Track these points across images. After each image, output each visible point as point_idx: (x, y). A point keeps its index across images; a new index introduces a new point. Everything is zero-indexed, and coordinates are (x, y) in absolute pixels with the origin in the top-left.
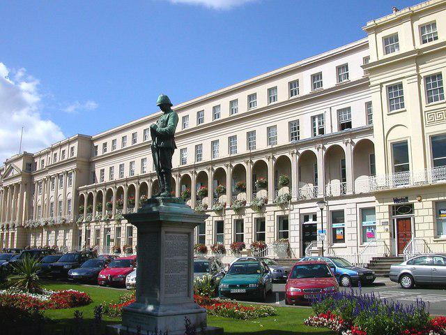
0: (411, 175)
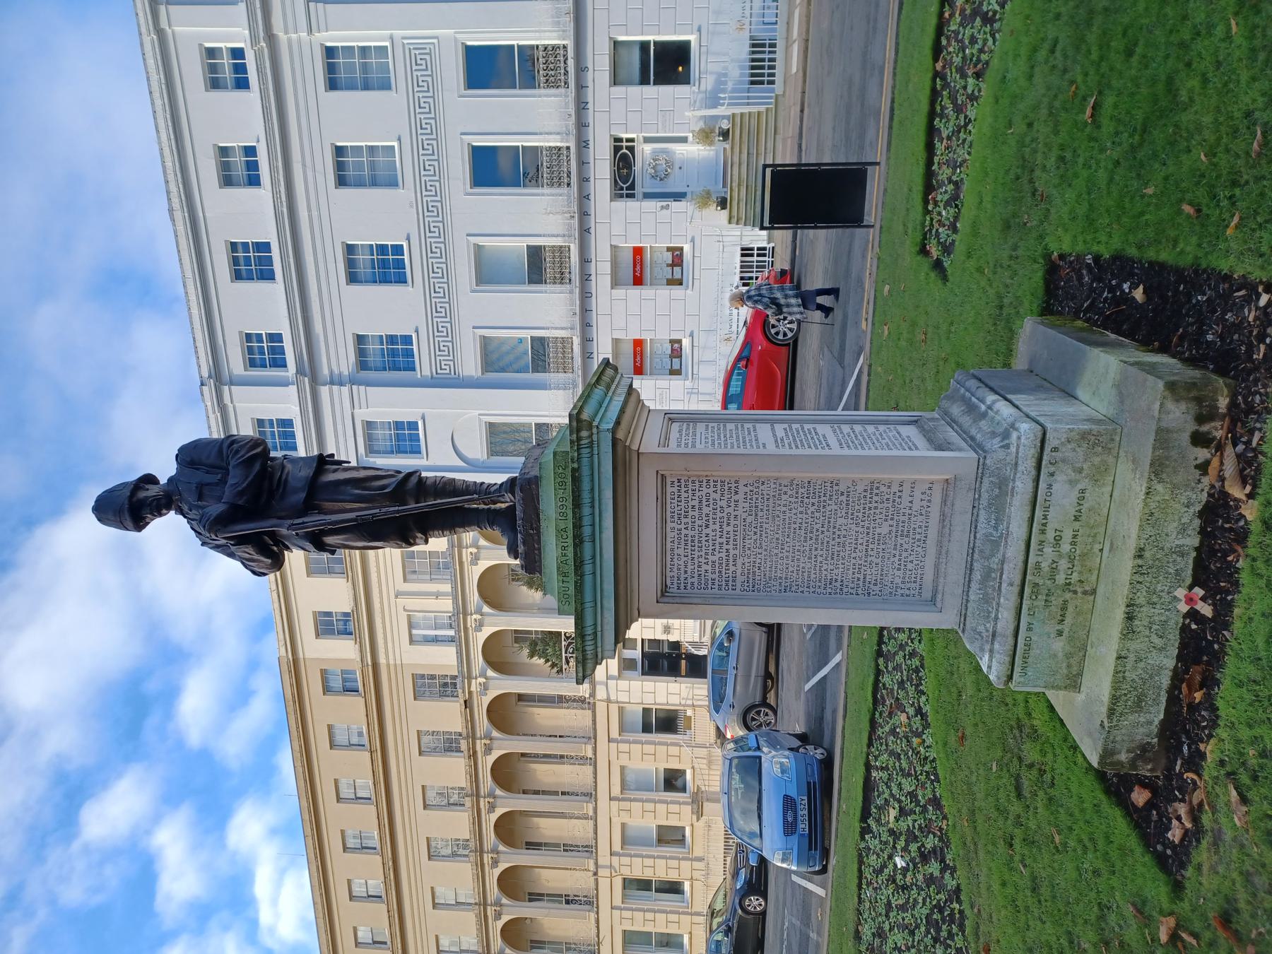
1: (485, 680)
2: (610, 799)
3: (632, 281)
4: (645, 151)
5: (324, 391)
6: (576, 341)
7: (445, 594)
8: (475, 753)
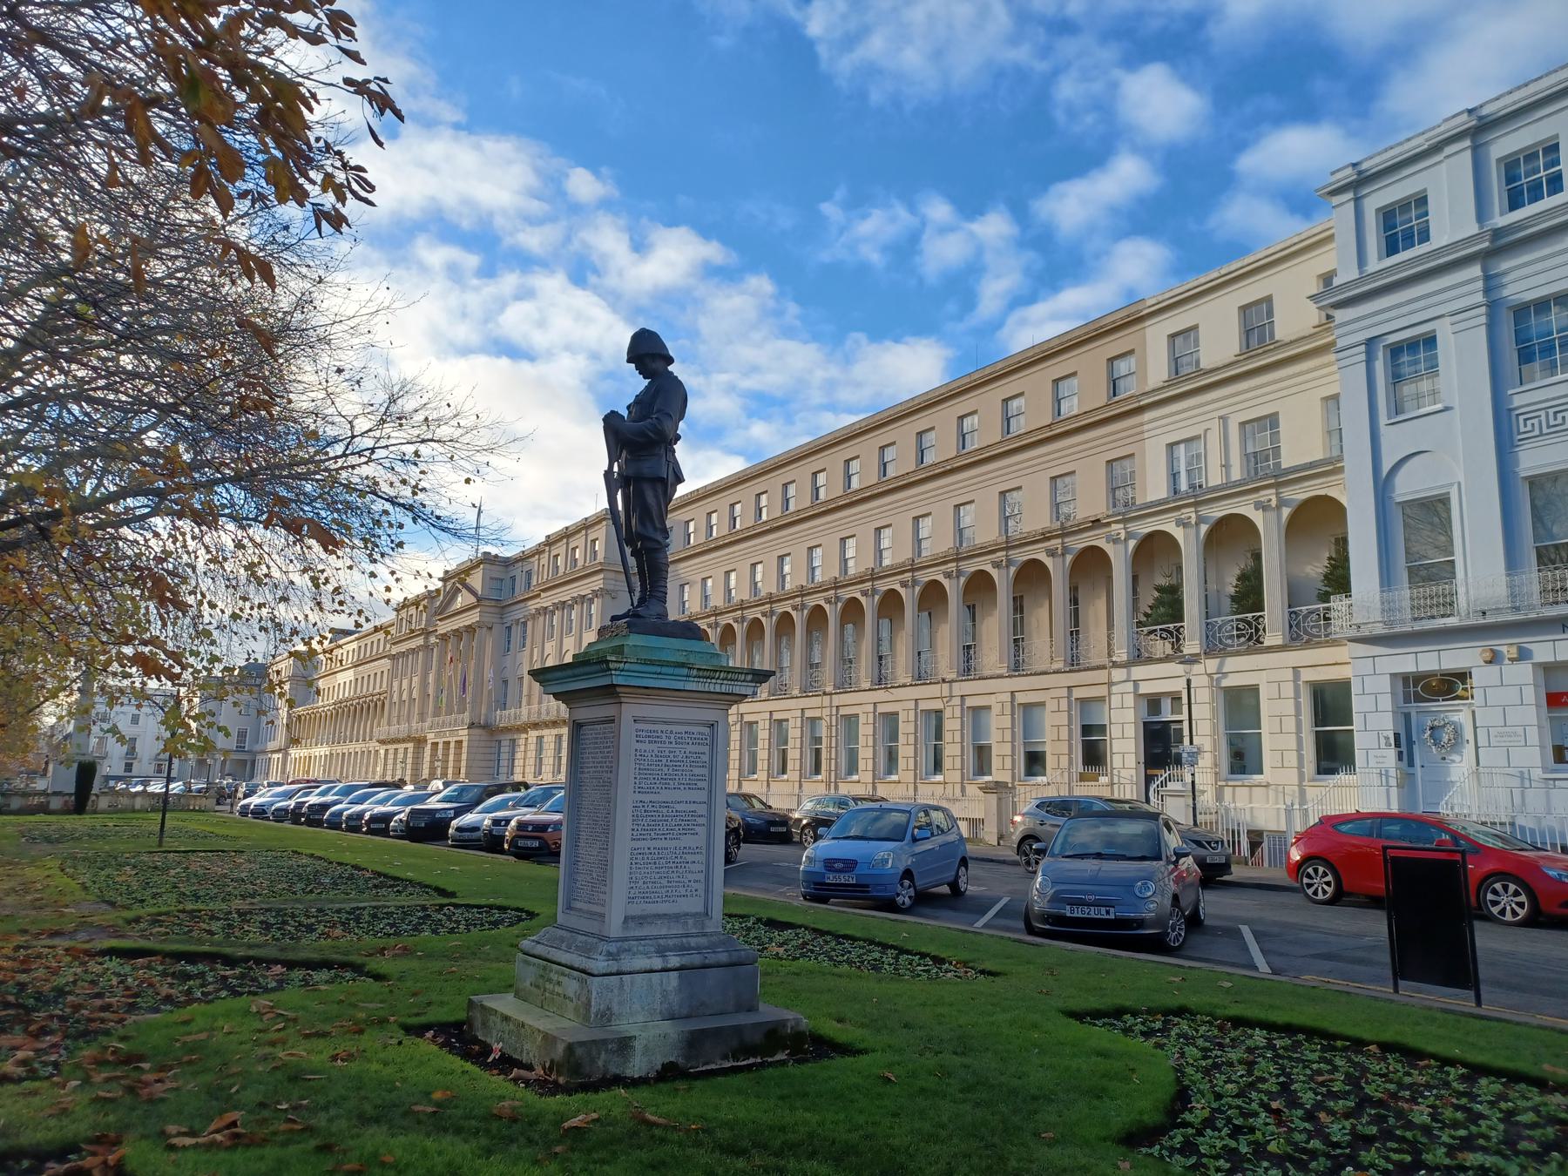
0: (1461, 590)
3: (1554, 690)
4: (1459, 714)
5: (1476, 271)
6: (1452, 621)
7: (1228, 474)
8: (1049, 539)
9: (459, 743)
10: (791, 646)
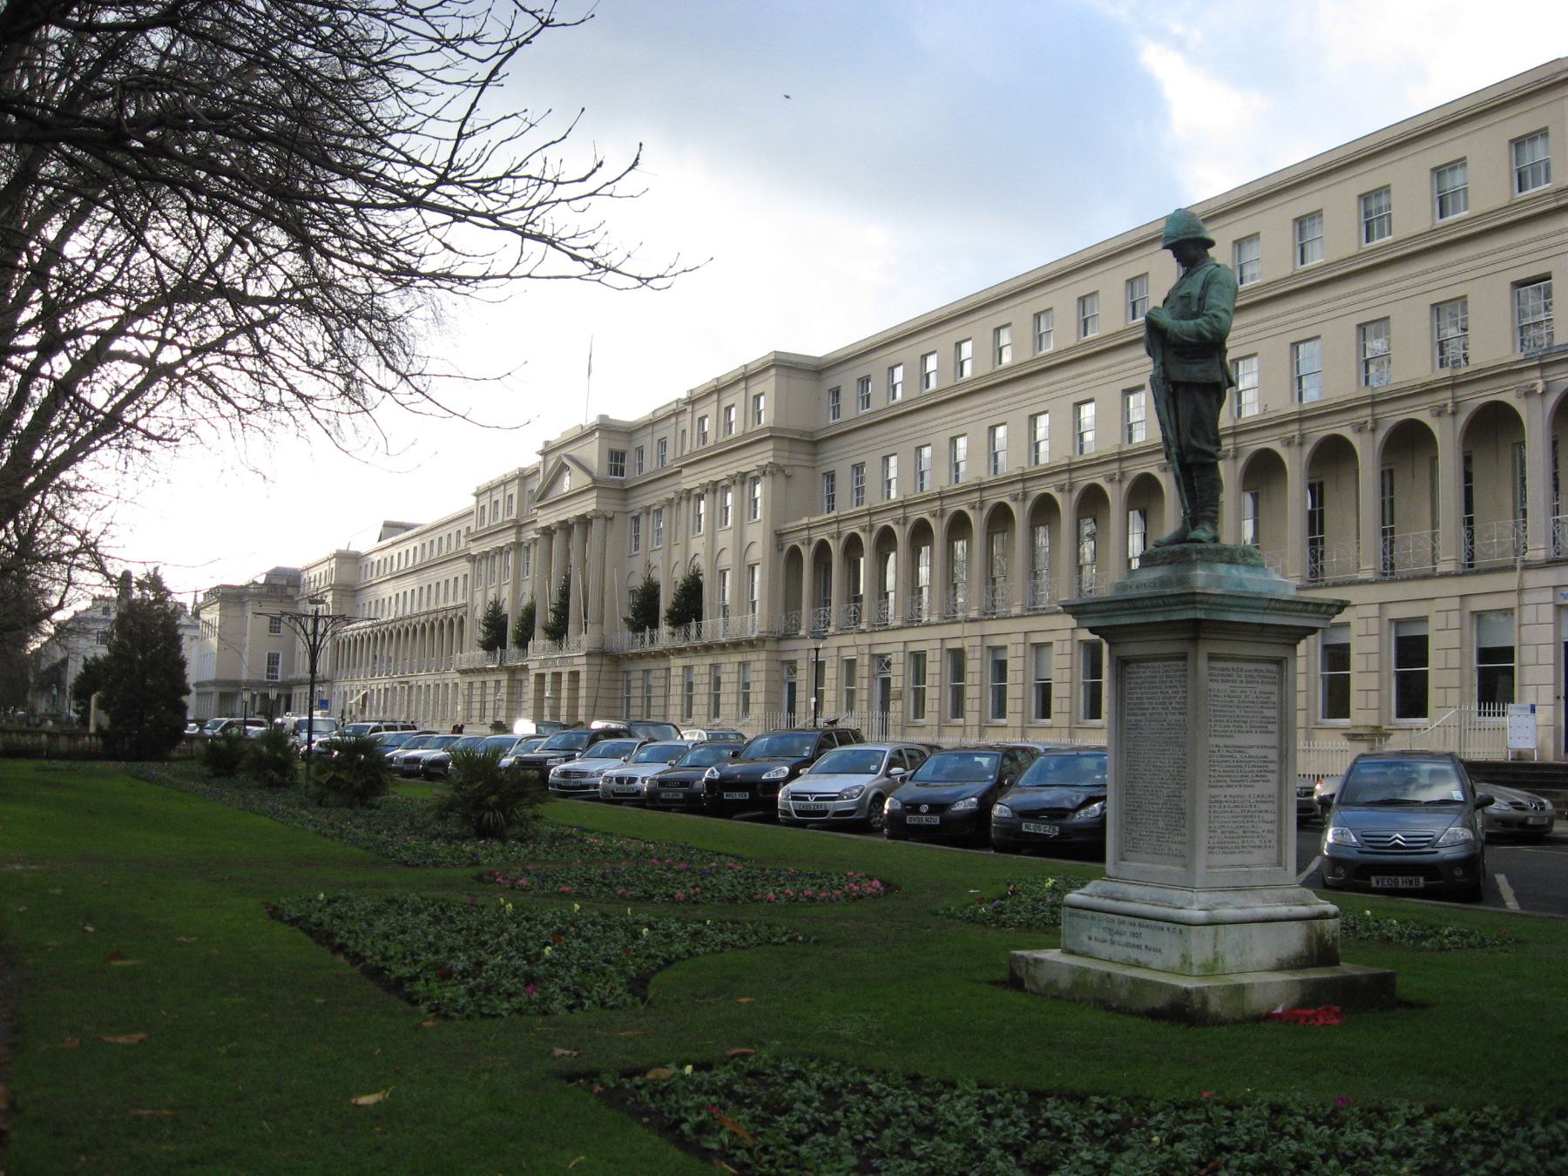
1: (1540, 391)
2: (1461, 596)
9: (575, 675)
10: (1008, 547)
